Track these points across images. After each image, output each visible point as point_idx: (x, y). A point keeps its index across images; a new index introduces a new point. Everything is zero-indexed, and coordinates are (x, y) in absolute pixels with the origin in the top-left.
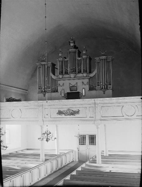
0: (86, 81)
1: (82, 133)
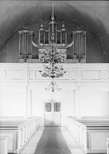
0: (64, 51)
1: (48, 101)
